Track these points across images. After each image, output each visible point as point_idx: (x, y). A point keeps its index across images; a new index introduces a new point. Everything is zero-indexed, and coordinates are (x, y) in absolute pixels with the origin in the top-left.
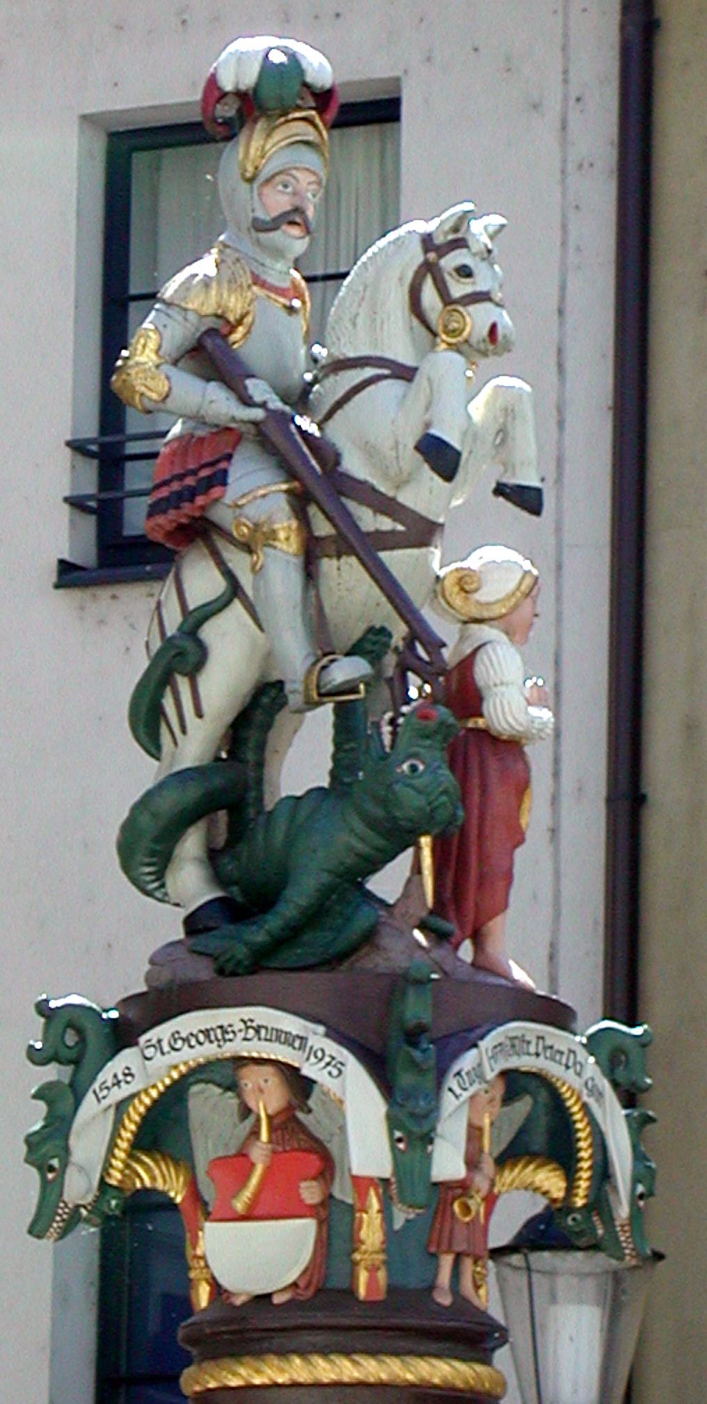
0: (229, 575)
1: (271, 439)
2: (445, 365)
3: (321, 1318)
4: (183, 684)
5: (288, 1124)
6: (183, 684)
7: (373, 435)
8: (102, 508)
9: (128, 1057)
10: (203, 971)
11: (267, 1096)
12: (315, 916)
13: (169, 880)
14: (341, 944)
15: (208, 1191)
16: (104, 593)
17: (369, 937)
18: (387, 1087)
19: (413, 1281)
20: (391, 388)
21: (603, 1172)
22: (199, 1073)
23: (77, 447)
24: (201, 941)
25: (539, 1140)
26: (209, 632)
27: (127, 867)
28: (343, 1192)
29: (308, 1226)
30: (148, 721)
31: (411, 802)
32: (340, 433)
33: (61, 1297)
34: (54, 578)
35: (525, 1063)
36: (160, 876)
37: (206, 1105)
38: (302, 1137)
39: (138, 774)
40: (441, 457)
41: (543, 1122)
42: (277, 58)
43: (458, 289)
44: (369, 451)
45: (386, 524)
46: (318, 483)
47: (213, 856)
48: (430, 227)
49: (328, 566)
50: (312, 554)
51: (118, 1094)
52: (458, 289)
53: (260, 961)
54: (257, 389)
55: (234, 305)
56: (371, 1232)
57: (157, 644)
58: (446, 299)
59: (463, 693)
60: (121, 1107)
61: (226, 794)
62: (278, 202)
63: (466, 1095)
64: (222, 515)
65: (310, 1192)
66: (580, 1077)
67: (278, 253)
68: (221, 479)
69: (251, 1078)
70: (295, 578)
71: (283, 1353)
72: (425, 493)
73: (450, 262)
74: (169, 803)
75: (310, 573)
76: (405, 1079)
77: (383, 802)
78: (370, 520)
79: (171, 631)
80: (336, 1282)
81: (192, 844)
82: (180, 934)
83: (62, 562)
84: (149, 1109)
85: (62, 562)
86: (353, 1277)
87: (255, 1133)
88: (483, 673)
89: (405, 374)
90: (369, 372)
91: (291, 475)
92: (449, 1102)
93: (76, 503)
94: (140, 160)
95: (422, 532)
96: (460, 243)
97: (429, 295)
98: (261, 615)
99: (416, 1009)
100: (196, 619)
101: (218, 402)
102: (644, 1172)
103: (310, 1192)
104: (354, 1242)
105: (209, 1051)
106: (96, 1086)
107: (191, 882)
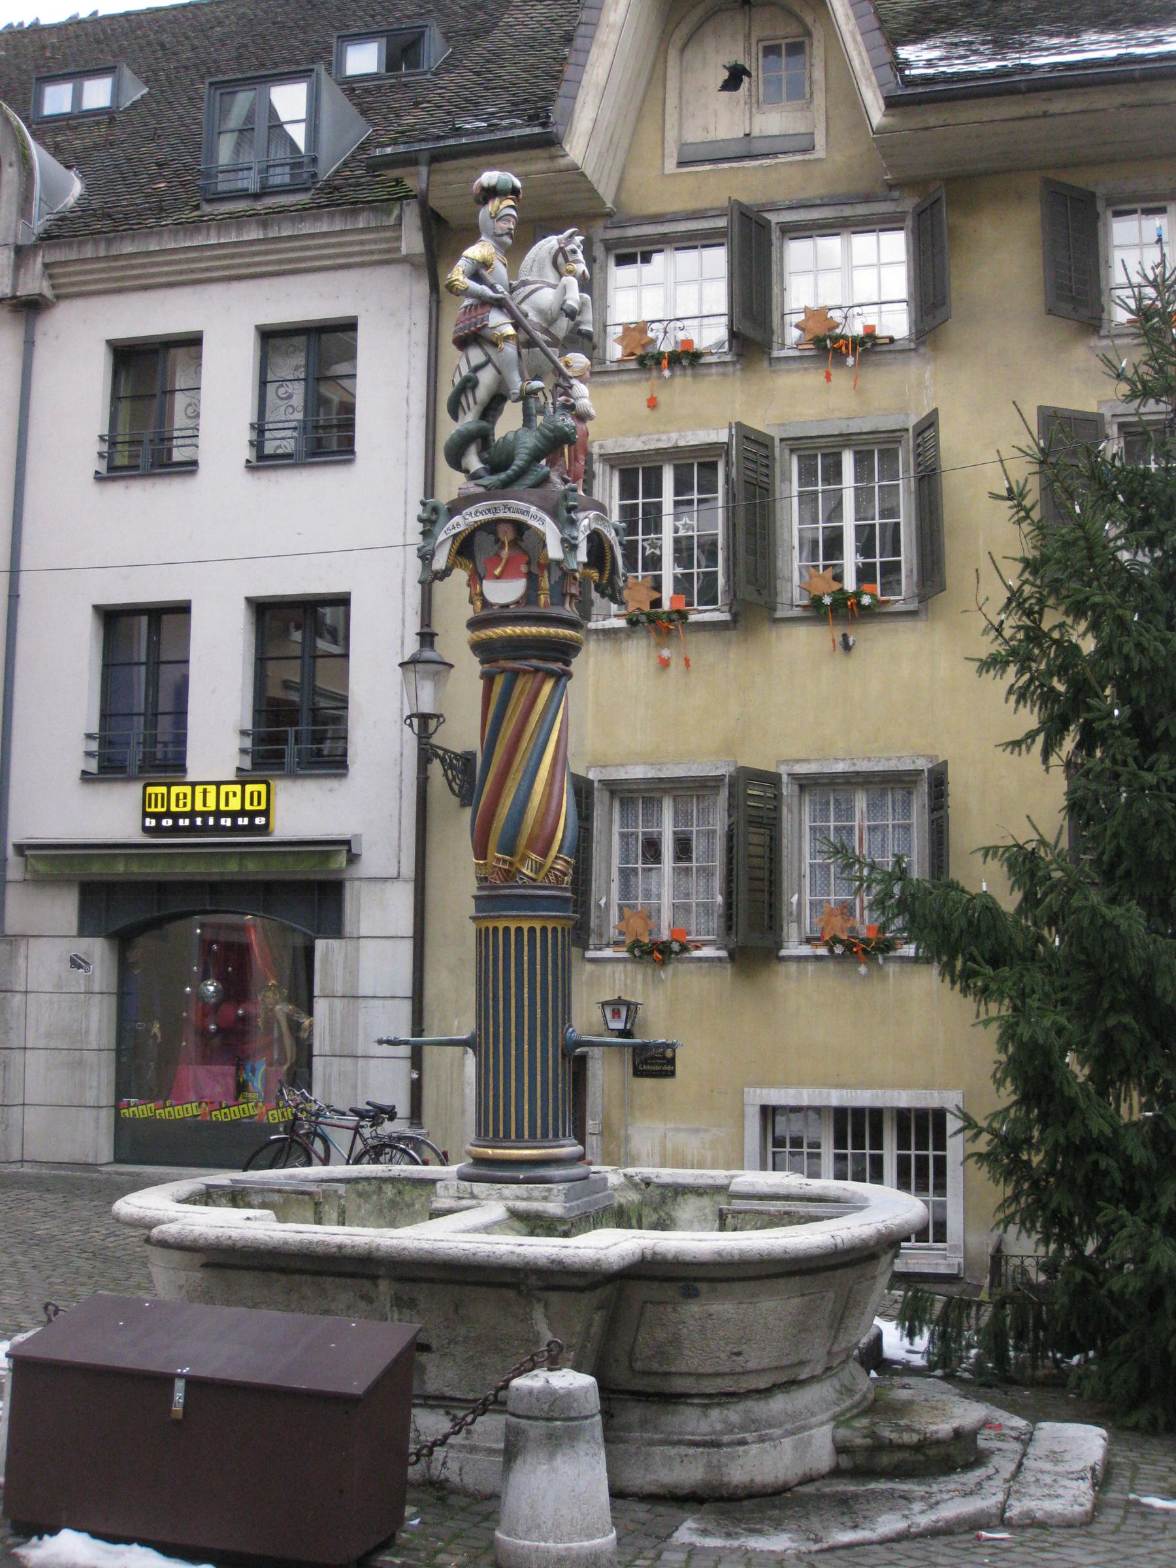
8: (257, 445)
9: (457, 519)
28: (535, 570)
54: (499, 287)
97: (560, 259)
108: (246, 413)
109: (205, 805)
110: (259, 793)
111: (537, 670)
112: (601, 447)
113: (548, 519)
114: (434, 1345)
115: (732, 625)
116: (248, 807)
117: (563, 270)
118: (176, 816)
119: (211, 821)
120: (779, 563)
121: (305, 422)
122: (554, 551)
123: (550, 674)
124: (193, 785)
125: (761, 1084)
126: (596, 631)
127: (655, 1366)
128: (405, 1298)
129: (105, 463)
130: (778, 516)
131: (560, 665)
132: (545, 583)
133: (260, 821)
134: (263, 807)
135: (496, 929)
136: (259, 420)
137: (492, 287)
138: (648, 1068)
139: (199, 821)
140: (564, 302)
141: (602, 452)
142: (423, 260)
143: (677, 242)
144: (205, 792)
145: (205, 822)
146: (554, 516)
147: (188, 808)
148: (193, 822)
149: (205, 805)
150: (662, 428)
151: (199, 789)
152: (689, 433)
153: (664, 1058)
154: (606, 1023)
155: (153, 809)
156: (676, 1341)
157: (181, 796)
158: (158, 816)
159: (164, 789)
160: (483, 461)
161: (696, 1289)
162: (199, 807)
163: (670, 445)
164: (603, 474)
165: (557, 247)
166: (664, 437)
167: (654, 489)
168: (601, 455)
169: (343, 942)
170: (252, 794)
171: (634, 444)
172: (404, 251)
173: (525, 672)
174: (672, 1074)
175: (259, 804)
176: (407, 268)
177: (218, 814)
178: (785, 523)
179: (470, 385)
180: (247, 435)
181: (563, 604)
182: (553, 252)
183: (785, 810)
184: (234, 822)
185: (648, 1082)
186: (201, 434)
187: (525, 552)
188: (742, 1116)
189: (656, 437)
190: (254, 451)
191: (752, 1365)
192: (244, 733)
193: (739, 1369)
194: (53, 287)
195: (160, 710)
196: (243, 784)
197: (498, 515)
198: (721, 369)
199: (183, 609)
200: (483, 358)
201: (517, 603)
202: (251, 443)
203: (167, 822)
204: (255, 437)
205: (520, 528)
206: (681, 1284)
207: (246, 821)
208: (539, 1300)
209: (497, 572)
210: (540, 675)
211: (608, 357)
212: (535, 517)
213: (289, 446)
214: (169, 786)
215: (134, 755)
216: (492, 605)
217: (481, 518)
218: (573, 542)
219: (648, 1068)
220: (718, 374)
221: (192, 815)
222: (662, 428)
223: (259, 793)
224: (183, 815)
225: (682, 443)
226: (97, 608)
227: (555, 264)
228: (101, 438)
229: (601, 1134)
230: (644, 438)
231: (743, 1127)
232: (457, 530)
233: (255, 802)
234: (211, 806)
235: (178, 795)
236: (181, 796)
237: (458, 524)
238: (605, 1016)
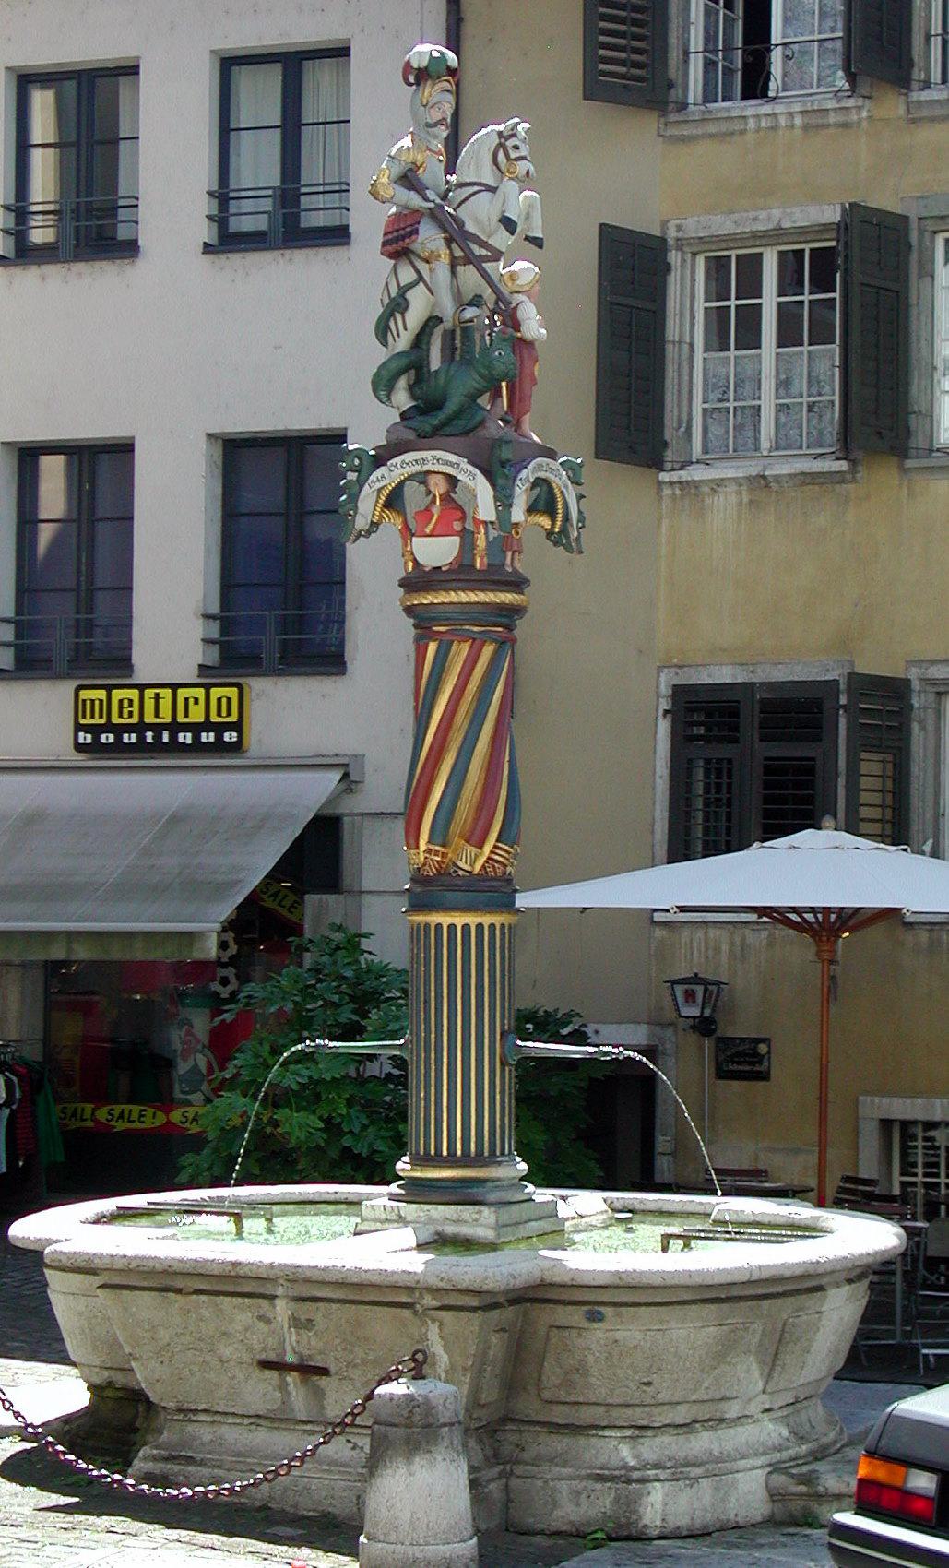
0: (418, 272)
1: (436, 215)
2: (510, 186)
3: (462, 577)
4: (398, 316)
5: (447, 498)
6: (398, 316)
7: (478, 215)
8: (220, 221)
9: (382, 470)
10: (411, 436)
11: (439, 487)
12: (458, 414)
13: (393, 398)
14: (470, 426)
15: (412, 524)
16: (223, 257)
17: (482, 423)
18: (493, 485)
19: (497, 562)
20: (486, 195)
21: (567, 518)
22: (410, 478)
23: (210, 193)
24: (409, 423)
25: (541, 505)
26: (409, 295)
27: (375, 391)
28: (470, 526)
29: (457, 539)
30: (383, 331)
31: (499, 368)
32: (462, 213)
33: (208, 551)
35: (542, 475)
36: (389, 396)
37: (412, 490)
38: (453, 506)
39: (380, 355)
40: (509, 224)
41: (544, 496)
42: (436, 54)
43: (513, 155)
44: (477, 221)
45: (484, 252)
46: (455, 233)
47: (411, 388)
48: (501, 127)
49: (460, 269)
50: (454, 264)
51: (379, 485)
52: (513, 155)
53: (436, 431)
54: (430, 194)
55: (420, 159)
56: (481, 542)
57: (386, 301)
58: (509, 159)
59: (513, 322)
60: (379, 490)
61: (414, 362)
62: (436, 116)
64: (416, 247)
65: (457, 526)
66: (560, 480)
67: (436, 137)
68: (416, 232)
69: (432, 480)
70: (448, 273)
71: (447, 590)
72: (501, 240)
73: (510, 143)
74: (394, 365)
75: (453, 273)
76: (501, 481)
77: (488, 368)
78: (478, 251)
79: (393, 295)
80: (466, 562)
81: (402, 383)
82: (398, 419)
86: (474, 559)
87: (434, 501)
88: (520, 314)
89: (493, 190)
91: (446, 231)
92: (518, 491)
93: (210, 218)
94: (235, 69)
95: (496, 255)
96: (514, 135)
97: (501, 156)
99: (506, 453)
100: (403, 291)
101: (415, 200)
102: (581, 518)
103: (457, 526)
104: (474, 546)
105: (418, 468)
107: (402, 399)
108: (203, 173)
109: (157, 715)
110: (229, 700)
112: (679, 228)
114: (333, 1369)
115: (849, 477)
116: (214, 719)
118: (119, 730)
119: (166, 738)
120: (914, 390)
121: (284, 191)
124: (141, 688)
125: (882, 1092)
127: (562, 1396)
128: (303, 1318)
130: (914, 327)
133: (230, 737)
134: (234, 718)
135: (439, 927)
138: (736, 1067)
139: (149, 736)
141: (680, 235)
144: (157, 697)
145: (158, 737)
147: (135, 720)
148: (141, 738)
149: (157, 715)
151: (149, 693)
152: (797, 210)
153: (756, 1054)
154: (678, 1010)
155: (88, 721)
156: (582, 1369)
157: (126, 703)
158: (96, 730)
159: (102, 694)
160: (413, 396)
161: (600, 1313)
162: (150, 718)
166: (762, 215)
167: (751, 285)
169: (341, 897)
170: (219, 700)
171: (724, 225)
174: (764, 1076)
175: (229, 714)
177: (175, 727)
178: (924, 334)
180: (205, 206)
183: (915, 727)
184: (196, 738)
185: (736, 1085)
186: (140, 203)
188: (856, 1132)
189: (752, 214)
191: (663, 1397)
192: (207, 617)
193: (649, 1401)
195: (99, 584)
196: (207, 687)
199: (123, 450)
200: (412, 276)
203: (107, 738)
206: (586, 1308)
207: (212, 737)
208: (433, 1320)
213: (262, 223)
214: (109, 688)
215: (60, 643)
219: (736, 1067)
221: (141, 728)
223: (229, 700)
224: (129, 728)
229: (673, 1154)
230: (736, 216)
231: (857, 1149)
233: (224, 712)
234: (166, 717)
235: (121, 701)
236: (126, 703)
238: (675, 999)
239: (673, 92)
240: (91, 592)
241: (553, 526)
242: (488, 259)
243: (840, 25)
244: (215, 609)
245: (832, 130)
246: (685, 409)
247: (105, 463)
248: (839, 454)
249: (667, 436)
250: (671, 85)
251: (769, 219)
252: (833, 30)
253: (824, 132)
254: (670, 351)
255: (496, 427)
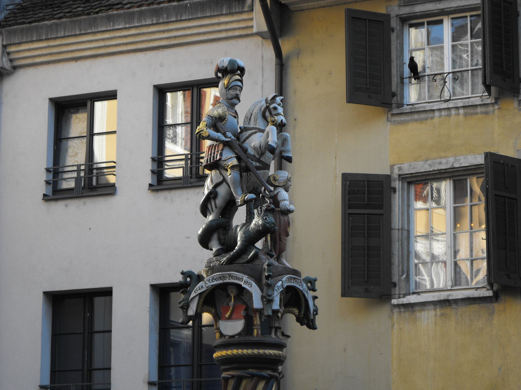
34: (148, 188)
43: (273, 113)
51: (199, 292)
54: (229, 134)
63: (279, 291)
83: (44, 194)
84: (207, 295)
85: (44, 194)
88: (280, 198)
90: (253, 131)
97: (267, 114)
98: (475, 307)
106: (195, 290)
107: (215, 246)
111: (253, 376)
112: (400, 169)
113: (254, 284)
115: (494, 299)
117: (269, 120)
122: (257, 304)
123: (262, 378)
126: (399, 306)
129: (51, 187)
131: (270, 372)
132: (257, 321)
136: (158, 155)
137: (224, 134)
140: (268, 142)
141: (401, 173)
142: (269, 35)
143: (453, 14)
146: (258, 282)
150: (443, 154)
152: (462, 158)
163: (448, 167)
164: (403, 189)
165: (265, 106)
166: (444, 161)
168: (399, 175)
172: (255, 30)
173: (246, 377)
176: (259, 39)
179: (212, 196)
181: (270, 334)
182: (263, 109)
187: (245, 303)
189: (438, 161)
190: (155, 177)
194: (11, 61)
197: (225, 281)
198: (484, 109)
201: (239, 334)
202: (153, 172)
204: (155, 168)
205: (239, 287)
209: (227, 315)
210: (255, 378)
211: (405, 102)
212: (246, 282)
216: (225, 336)
217: (215, 283)
218: (269, 298)
220: (482, 113)
222: (443, 154)
225: (457, 165)
226: (47, 294)
227: (264, 117)
228: (48, 170)
230: (430, 162)
232: (202, 291)
237: (202, 287)
239: (395, 98)
240: (91, 370)
241: (300, 312)
242: (258, 168)
243: (480, 61)
244: (155, 378)
245: (479, 116)
246: (406, 265)
247: (98, 301)
248: (489, 287)
249: (395, 279)
250: (394, 95)
251: (447, 163)
252: (477, 65)
253: (476, 116)
254: (396, 235)
255: (265, 261)
